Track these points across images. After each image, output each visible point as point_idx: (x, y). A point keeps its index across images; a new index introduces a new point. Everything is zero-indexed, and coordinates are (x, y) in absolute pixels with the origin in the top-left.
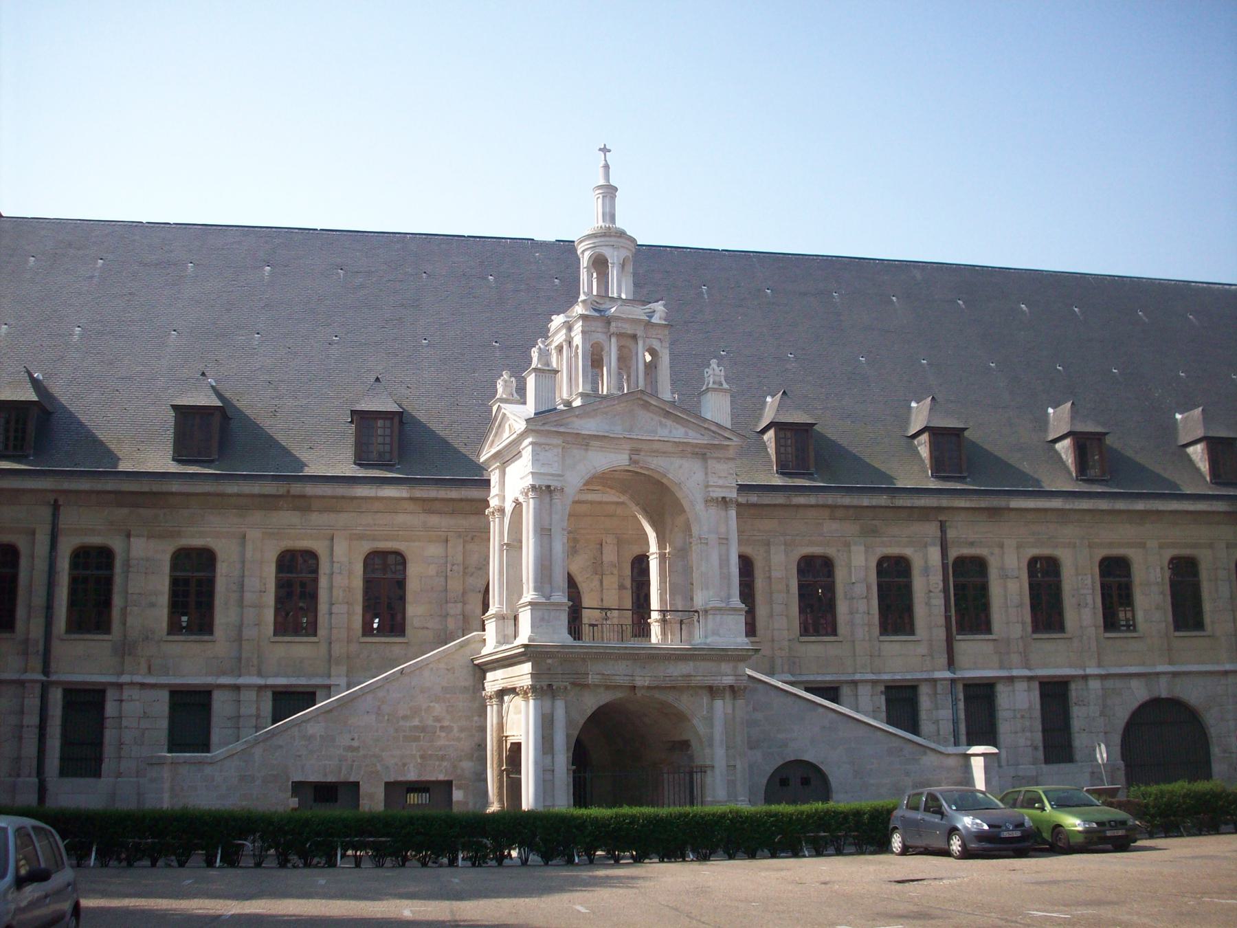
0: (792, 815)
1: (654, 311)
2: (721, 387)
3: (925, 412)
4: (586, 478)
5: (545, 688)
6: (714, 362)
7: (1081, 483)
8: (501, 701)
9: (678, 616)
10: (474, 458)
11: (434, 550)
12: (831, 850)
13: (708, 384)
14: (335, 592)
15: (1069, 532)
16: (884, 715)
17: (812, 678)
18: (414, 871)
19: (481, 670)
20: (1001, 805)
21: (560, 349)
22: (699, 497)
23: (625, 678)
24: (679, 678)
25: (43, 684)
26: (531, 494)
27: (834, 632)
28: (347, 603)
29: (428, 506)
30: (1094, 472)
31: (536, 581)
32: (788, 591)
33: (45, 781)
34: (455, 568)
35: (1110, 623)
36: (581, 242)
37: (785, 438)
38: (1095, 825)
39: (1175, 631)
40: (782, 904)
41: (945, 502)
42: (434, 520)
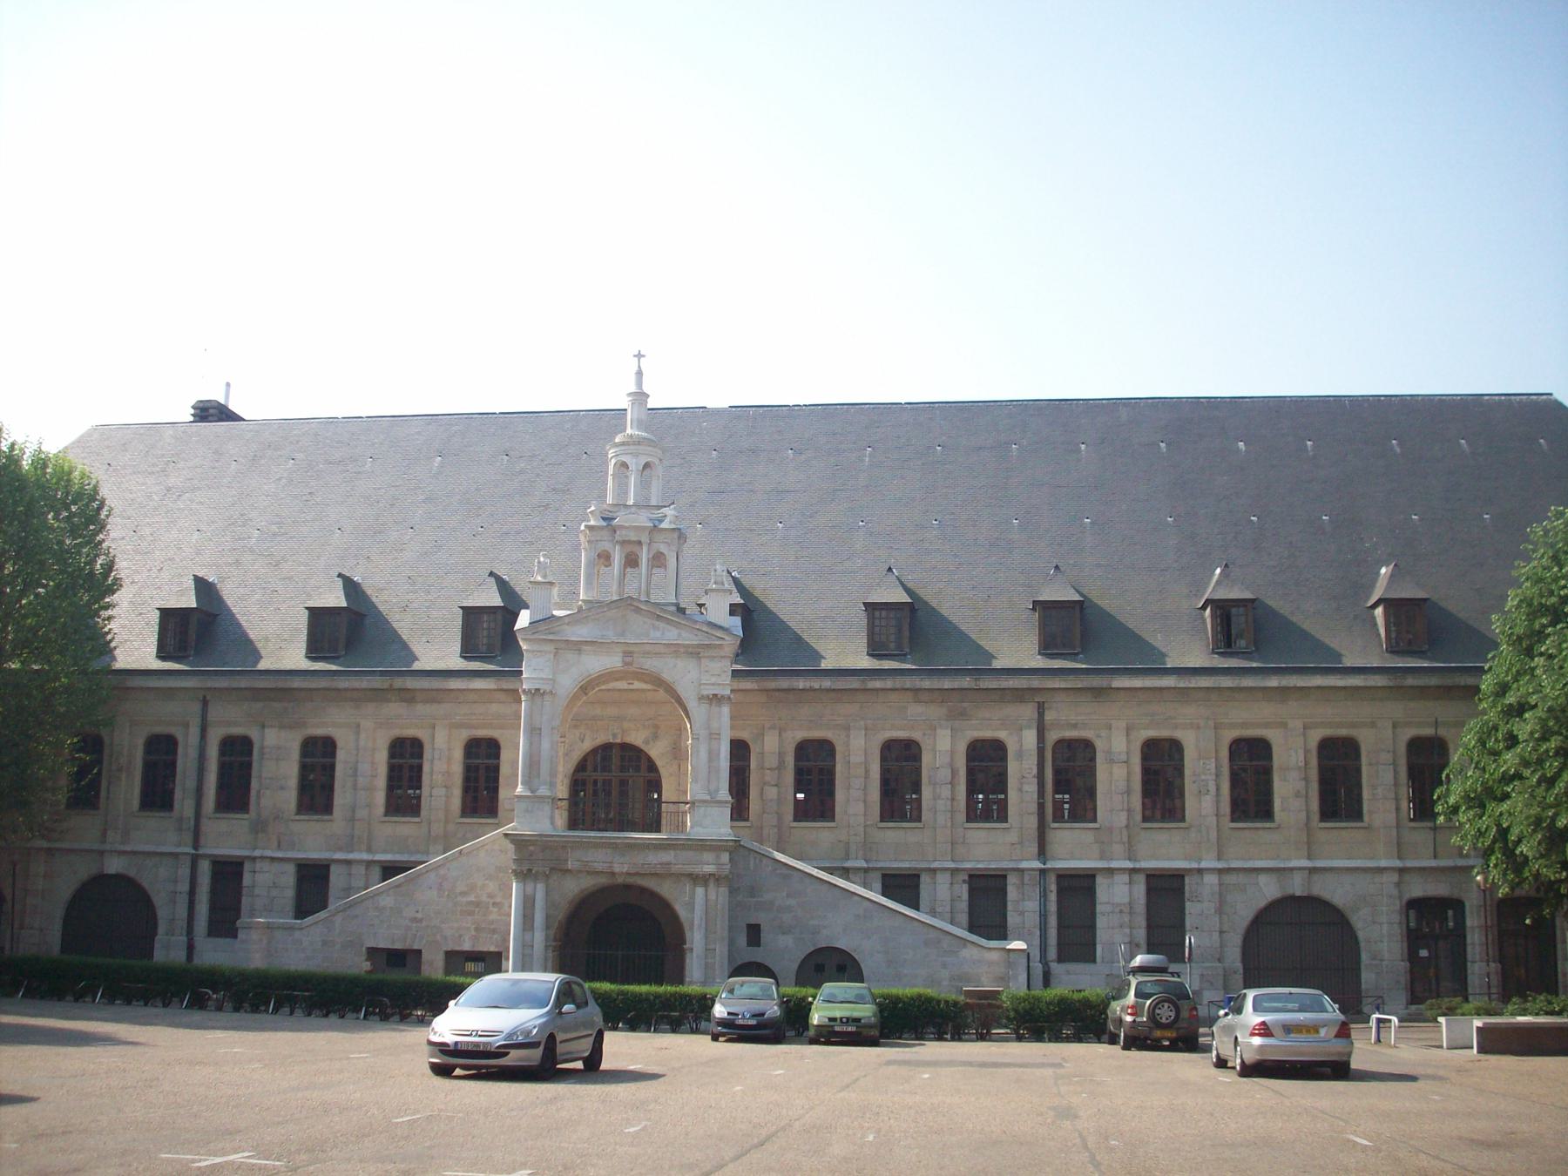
1: (666, 516)
7: (1216, 656)
12: (397, 1018)
15: (1190, 712)
17: (887, 865)
23: (605, 865)
28: (446, 787)
33: (192, 939)
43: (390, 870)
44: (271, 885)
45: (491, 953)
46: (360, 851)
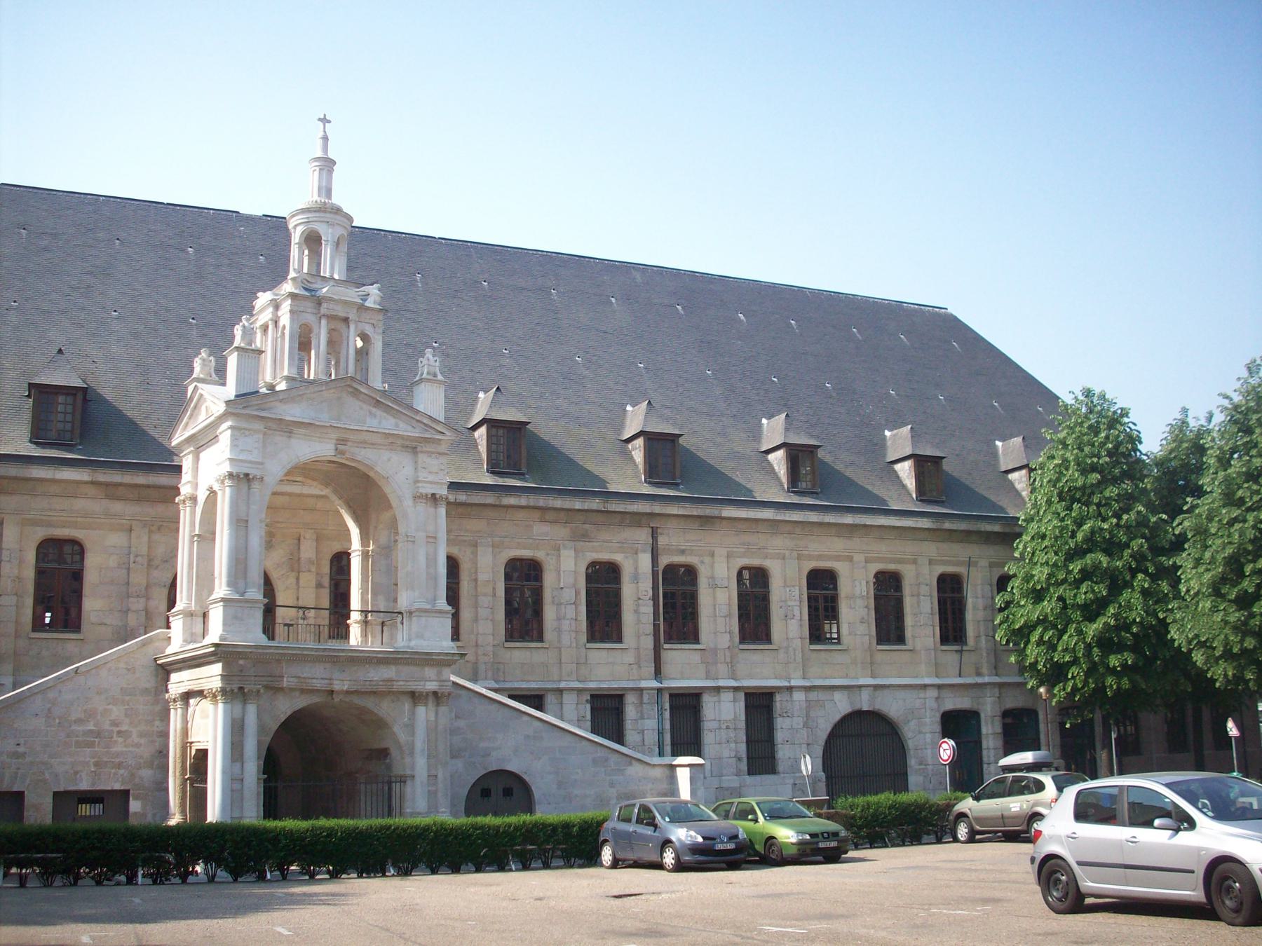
0: (499, 827)
1: (369, 295)
2: (435, 378)
3: (642, 417)
4: (289, 467)
5: (236, 690)
6: (429, 352)
8: (187, 704)
9: (380, 618)
10: (165, 442)
11: (116, 539)
13: (422, 374)
16: (589, 724)
17: (516, 685)
18: (87, 892)
19: (165, 671)
20: (715, 817)
21: (265, 328)
22: (407, 494)
23: (323, 682)
24: (381, 683)
26: (228, 482)
27: (540, 638)
28: (16, 594)
29: (111, 491)
30: (803, 485)
31: (230, 575)
32: (494, 595)
34: (139, 559)
35: (817, 635)
36: (294, 216)
37: (497, 436)
38: (808, 837)
39: (878, 644)
40: (500, 922)
41: (657, 508)
42: (118, 507)
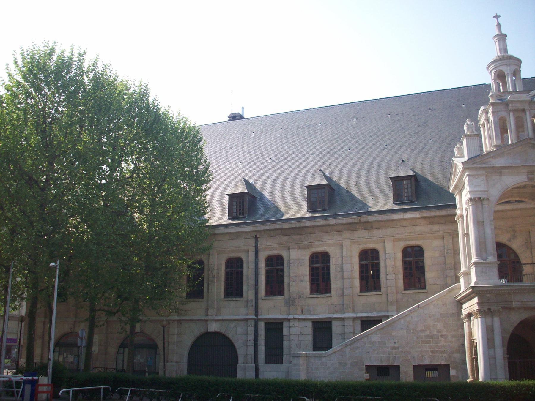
5: (486, 311)
8: (470, 320)
11: (437, 243)
14: (388, 269)
17: (364, 315)
19: (460, 303)
25: (255, 320)
26: (470, 203)
33: (258, 365)
34: (449, 251)
42: (436, 227)
43: (367, 323)
44: (300, 334)
45: (443, 365)
46: (348, 312)
